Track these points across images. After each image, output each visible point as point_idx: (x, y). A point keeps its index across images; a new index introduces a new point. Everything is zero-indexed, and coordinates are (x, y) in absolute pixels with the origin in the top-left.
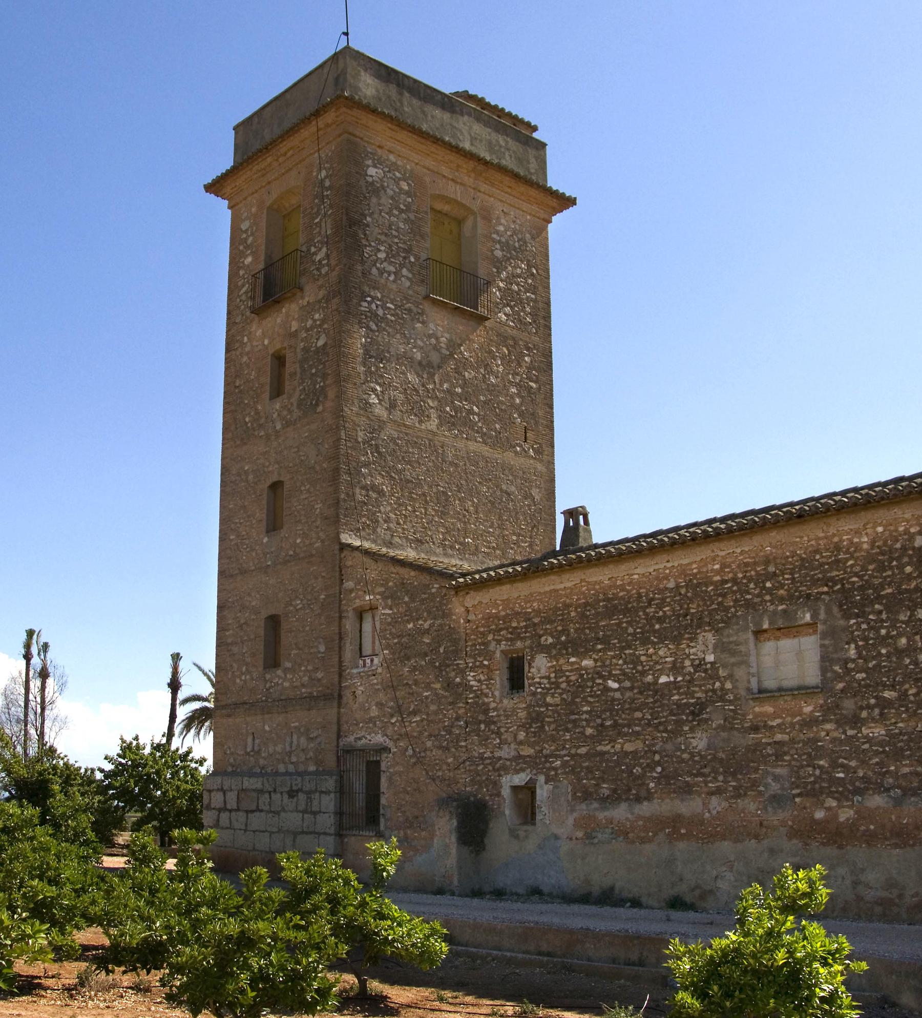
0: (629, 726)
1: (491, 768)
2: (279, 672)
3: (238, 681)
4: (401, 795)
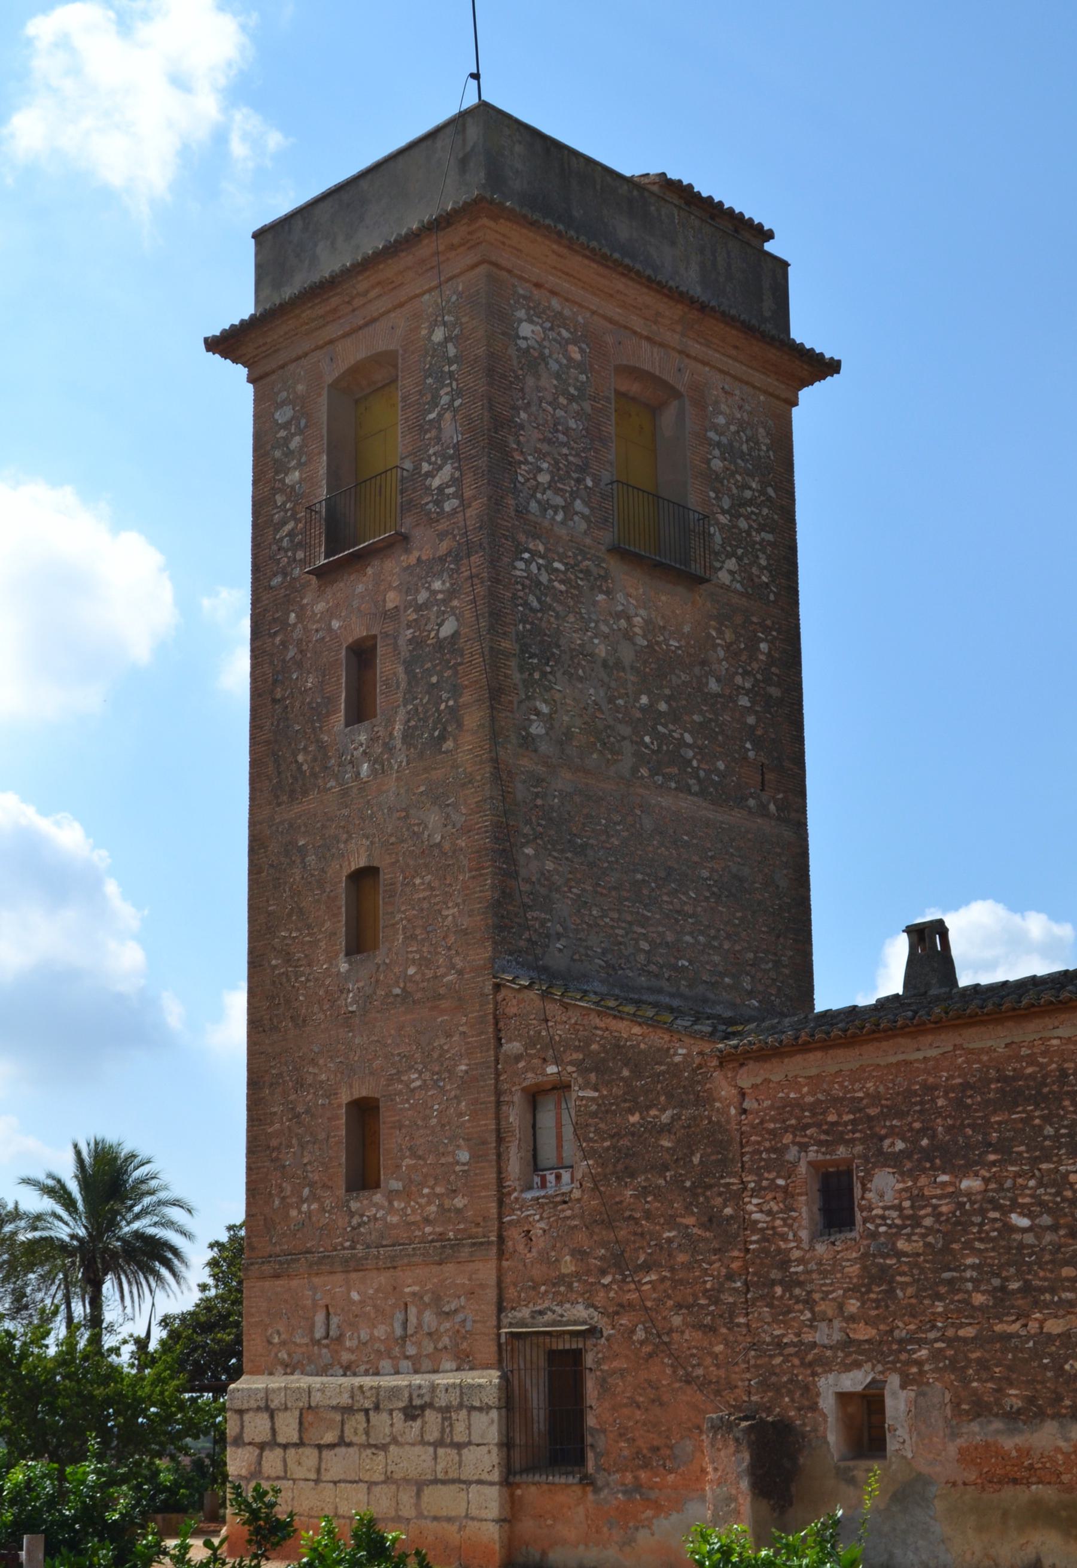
0: (1053, 1291)
1: (796, 1362)
2: (378, 1197)
3: (294, 1213)
4: (626, 1411)
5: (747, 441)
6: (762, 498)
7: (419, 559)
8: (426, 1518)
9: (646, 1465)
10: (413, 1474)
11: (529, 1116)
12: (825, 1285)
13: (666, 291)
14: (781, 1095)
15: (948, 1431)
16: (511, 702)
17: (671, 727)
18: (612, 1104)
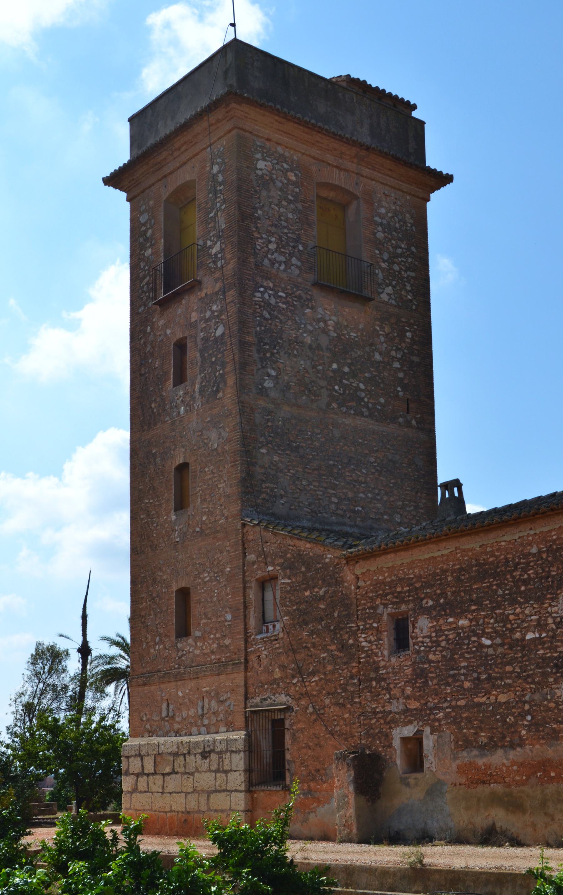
0: (501, 679)
1: (382, 721)
2: (190, 641)
4: (304, 751)
5: (399, 222)
6: (408, 253)
7: (206, 294)
8: (212, 811)
9: (313, 780)
10: (206, 787)
11: (260, 594)
12: (395, 680)
13: (345, 140)
14: (375, 578)
15: (452, 756)
16: (253, 370)
17: (351, 380)
18: (297, 586)
